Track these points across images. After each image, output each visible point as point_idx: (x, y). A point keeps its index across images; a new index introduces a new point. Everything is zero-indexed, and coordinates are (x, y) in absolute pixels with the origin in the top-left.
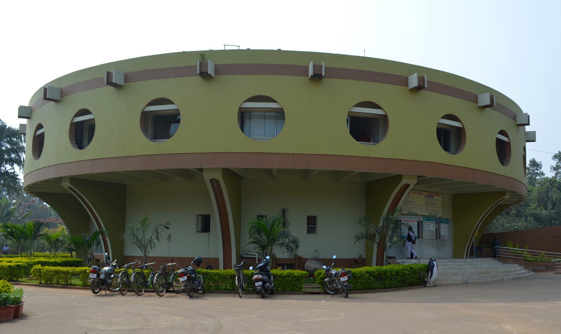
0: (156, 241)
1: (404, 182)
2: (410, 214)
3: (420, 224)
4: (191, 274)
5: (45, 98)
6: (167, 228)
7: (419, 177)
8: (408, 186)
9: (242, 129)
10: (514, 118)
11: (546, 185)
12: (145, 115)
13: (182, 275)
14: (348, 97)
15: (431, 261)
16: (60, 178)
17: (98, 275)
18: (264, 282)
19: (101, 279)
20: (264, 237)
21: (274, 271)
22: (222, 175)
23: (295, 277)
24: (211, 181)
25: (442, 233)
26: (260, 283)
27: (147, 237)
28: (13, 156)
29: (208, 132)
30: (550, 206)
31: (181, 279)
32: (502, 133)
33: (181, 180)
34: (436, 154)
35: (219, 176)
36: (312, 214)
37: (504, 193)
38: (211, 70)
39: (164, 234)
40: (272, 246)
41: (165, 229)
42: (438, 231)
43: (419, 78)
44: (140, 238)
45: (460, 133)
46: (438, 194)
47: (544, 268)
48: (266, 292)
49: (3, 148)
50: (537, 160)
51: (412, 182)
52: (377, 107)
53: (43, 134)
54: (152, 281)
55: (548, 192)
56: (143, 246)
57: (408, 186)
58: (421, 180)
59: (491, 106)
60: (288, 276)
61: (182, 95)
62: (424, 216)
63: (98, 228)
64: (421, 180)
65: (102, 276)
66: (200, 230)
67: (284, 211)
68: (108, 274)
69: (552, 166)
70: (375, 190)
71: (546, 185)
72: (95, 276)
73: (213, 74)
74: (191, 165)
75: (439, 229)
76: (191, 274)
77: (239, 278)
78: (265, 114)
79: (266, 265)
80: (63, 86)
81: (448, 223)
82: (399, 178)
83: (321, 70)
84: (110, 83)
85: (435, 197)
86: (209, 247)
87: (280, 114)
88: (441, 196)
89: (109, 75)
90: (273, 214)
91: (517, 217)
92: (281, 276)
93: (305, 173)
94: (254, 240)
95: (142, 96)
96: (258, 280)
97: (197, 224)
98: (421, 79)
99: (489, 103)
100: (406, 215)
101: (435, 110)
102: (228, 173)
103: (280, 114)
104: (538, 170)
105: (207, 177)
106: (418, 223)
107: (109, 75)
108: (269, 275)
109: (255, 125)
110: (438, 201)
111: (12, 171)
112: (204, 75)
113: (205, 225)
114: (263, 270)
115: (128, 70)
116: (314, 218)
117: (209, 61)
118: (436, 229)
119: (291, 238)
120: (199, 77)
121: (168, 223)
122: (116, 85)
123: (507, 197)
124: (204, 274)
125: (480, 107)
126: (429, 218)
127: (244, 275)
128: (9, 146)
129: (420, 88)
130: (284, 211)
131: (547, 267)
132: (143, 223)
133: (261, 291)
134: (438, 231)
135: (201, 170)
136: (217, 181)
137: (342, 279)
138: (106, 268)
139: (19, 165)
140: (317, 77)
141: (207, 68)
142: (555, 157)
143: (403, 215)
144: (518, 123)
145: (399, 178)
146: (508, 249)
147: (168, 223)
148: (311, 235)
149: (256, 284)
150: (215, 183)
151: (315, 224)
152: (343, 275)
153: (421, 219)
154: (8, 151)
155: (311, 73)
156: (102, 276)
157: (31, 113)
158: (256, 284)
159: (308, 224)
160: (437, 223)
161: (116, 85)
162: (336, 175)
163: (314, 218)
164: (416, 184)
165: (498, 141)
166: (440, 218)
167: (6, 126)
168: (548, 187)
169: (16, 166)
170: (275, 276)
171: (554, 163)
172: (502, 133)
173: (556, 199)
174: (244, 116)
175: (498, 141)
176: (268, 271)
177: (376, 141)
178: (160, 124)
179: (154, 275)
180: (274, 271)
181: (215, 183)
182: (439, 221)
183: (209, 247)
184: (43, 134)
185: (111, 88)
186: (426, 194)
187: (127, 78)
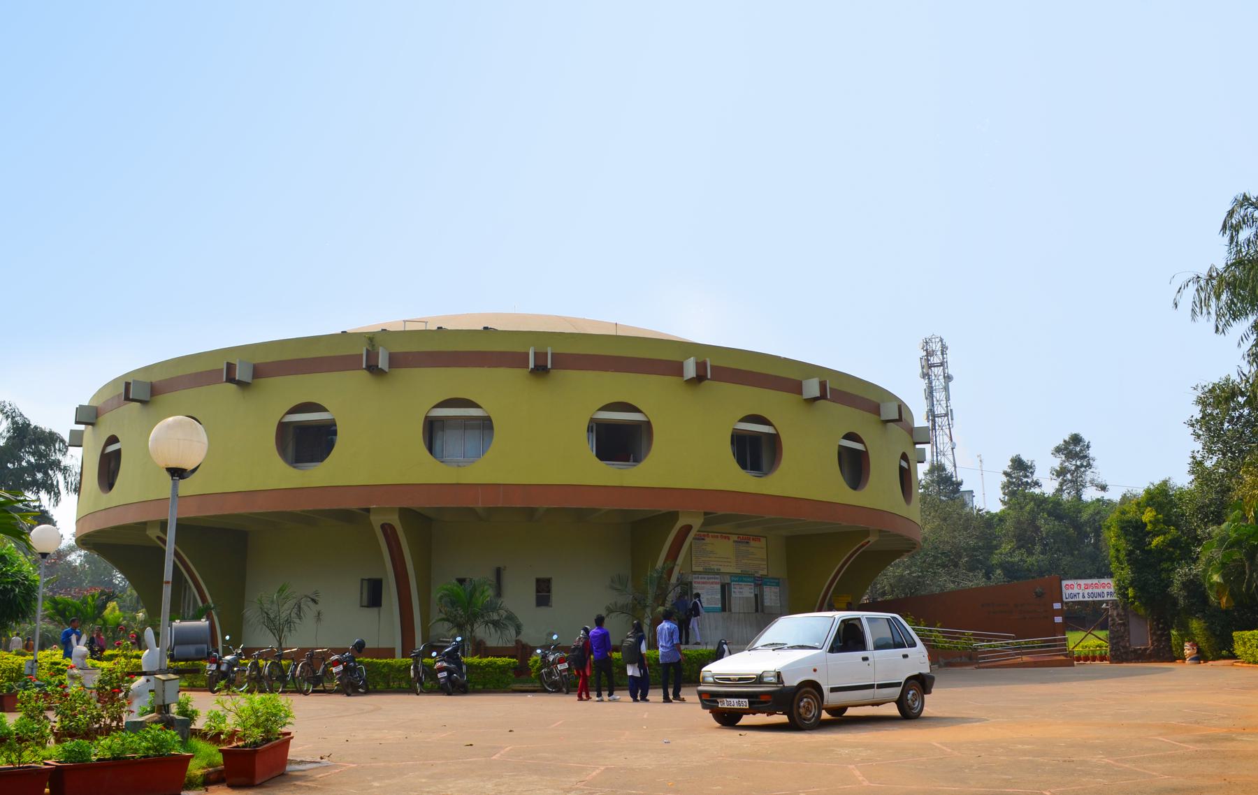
0: (297, 621)
1: (681, 522)
2: (707, 572)
3: (725, 589)
4: (348, 662)
5: (127, 398)
6: (314, 601)
7: (706, 514)
8: (688, 528)
9: (431, 450)
10: (875, 409)
11: (1028, 508)
12: (283, 427)
13: (336, 663)
14: (590, 395)
15: (720, 644)
16: (145, 523)
17: (218, 667)
18: (450, 672)
19: (222, 672)
20: (461, 612)
21: (469, 660)
22: (400, 518)
23: (500, 667)
24: (383, 526)
25: (767, 603)
26: (445, 674)
27: (284, 616)
28: (39, 476)
29: (379, 451)
30: (1038, 548)
31: (334, 670)
32: (851, 436)
33: (338, 525)
34: (730, 477)
35: (395, 520)
36: (543, 575)
37: (866, 533)
38: (383, 363)
39: (309, 610)
40: (472, 626)
41: (311, 604)
42: (758, 599)
43: (697, 364)
44: (272, 616)
45: (774, 440)
46: (757, 538)
47: (964, 659)
48: (455, 687)
49: (24, 464)
50: (1025, 458)
51: (697, 523)
52: (635, 409)
53: (118, 452)
54: (293, 675)
55: (1033, 521)
56: (277, 627)
57: (688, 528)
58: (711, 519)
59: (823, 396)
60: (487, 666)
61: (339, 398)
62: (731, 575)
63: (200, 604)
64: (711, 519)
65: (223, 668)
66: (365, 603)
67: (498, 572)
68: (231, 665)
69: (1053, 469)
70: (642, 537)
71: (1028, 508)
72: (214, 667)
73: (386, 368)
74: (353, 505)
75: (762, 595)
76: (348, 662)
77: (416, 668)
78: (466, 423)
79: (455, 650)
80: (155, 378)
81: (778, 584)
82: (673, 516)
83: (547, 358)
84: (231, 379)
85: (752, 543)
86: (380, 629)
87: (486, 425)
88: (763, 540)
89: (230, 367)
90: (480, 573)
91: (970, 570)
92: (478, 667)
93: (530, 513)
94: (443, 616)
95: (280, 399)
96: (441, 670)
97: (881, 686)
98: (701, 366)
99: (818, 394)
100: (700, 573)
101: (730, 408)
102: (408, 514)
103: (486, 425)
104: (1026, 476)
105: (376, 520)
106: (723, 587)
107: (230, 367)
108: (459, 665)
109: (451, 442)
110: (758, 549)
111: (37, 504)
112: (373, 369)
113: (374, 597)
114: (452, 657)
115: (260, 359)
116: (548, 581)
117: (381, 350)
118: (756, 596)
119: (502, 612)
120: (365, 373)
121: (316, 593)
122: (240, 384)
123: (872, 539)
124: (367, 665)
125: (806, 400)
126: (742, 577)
127: (424, 665)
128: (32, 460)
129: (700, 378)
130: (498, 572)
131: (970, 658)
132: (281, 591)
133: (445, 684)
134: (758, 599)
135: (368, 510)
136: (392, 527)
137: (560, 667)
138: (228, 658)
139: (49, 493)
140: (540, 370)
141: (376, 357)
142: (1058, 450)
143: (695, 573)
144: (884, 417)
145: (673, 516)
146: (1055, 640)
147: (316, 593)
148: (543, 610)
149: (439, 675)
150: (388, 530)
151: (549, 591)
152: (561, 661)
153: (728, 581)
154: (33, 468)
155: (531, 365)
156: (223, 668)
157: (97, 416)
158: (439, 675)
159: (538, 591)
160: (756, 585)
161: (240, 384)
162: (580, 515)
163: (548, 581)
164: (703, 525)
165: (901, 468)
166: (761, 578)
167: (29, 425)
168: (1032, 510)
169: (43, 495)
170: (470, 666)
171: (1057, 462)
172: (851, 436)
173: (1047, 534)
174: (432, 428)
175: (901, 468)
176: (458, 658)
177: (637, 460)
178: (307, 440)
179: (296, 667)
180: (469, 660)
181: (388, 530)
182: (760, 582)
183: (380, 629)
184: (118, 452)
185: (232, 386)
186: (735, 538)
187: (259, 372)
